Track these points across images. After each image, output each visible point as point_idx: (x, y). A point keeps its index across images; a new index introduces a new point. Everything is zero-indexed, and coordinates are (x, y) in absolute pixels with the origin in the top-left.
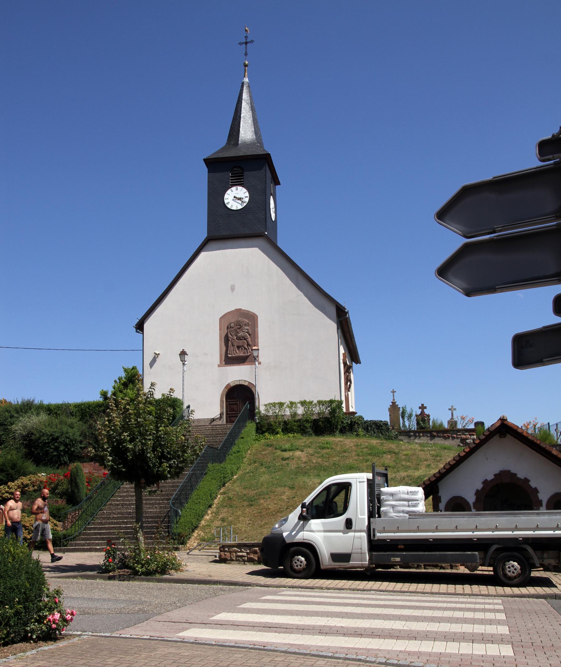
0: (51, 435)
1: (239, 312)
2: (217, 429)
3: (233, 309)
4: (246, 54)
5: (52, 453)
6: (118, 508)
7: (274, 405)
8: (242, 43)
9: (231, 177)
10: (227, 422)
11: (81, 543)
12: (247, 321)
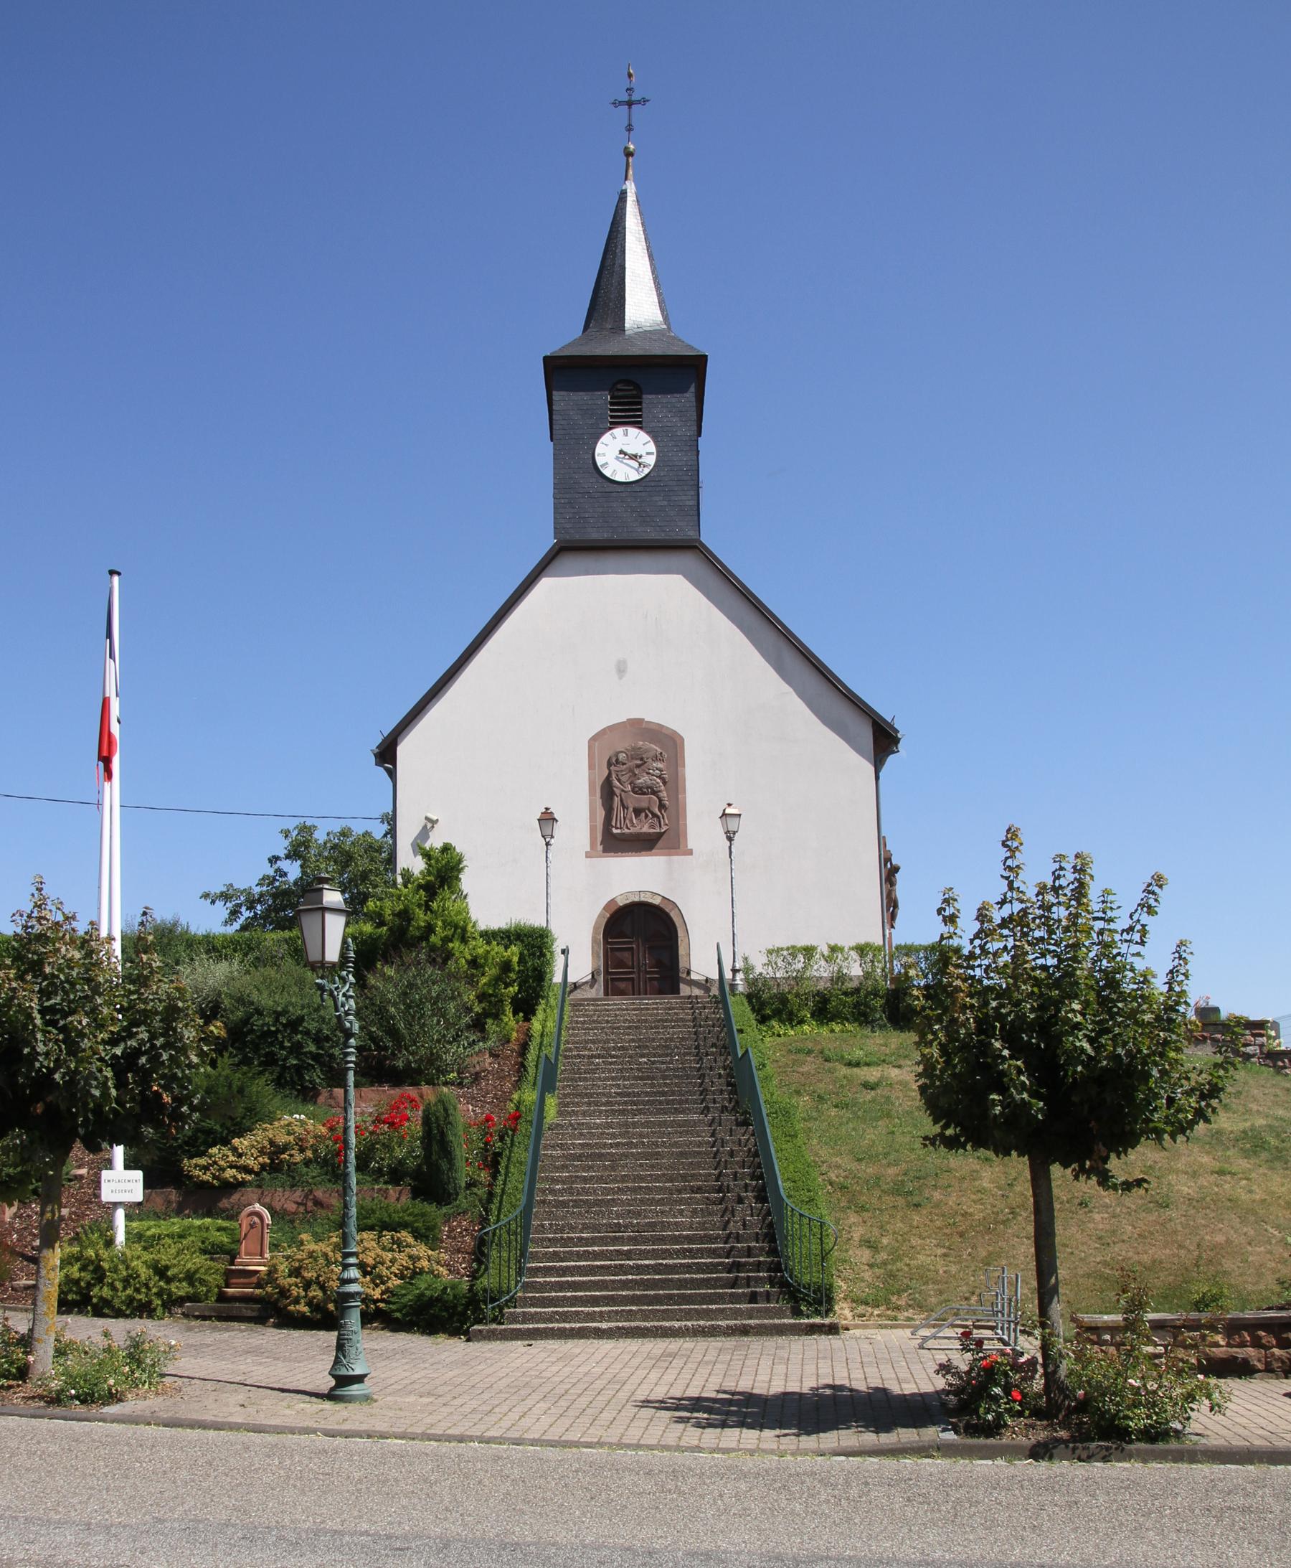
0: (285, 1012)
1: (637, 727)
2: (648, 1009)
3: (623, 718)
4: (629, 128)
5: (285, 1060)
6: (574, 1213)
7: (794, 952)
8: (621, 103)
9: (612, 404)
10: (606, 993)
11: (541, 1313)
12: (659, 750)
